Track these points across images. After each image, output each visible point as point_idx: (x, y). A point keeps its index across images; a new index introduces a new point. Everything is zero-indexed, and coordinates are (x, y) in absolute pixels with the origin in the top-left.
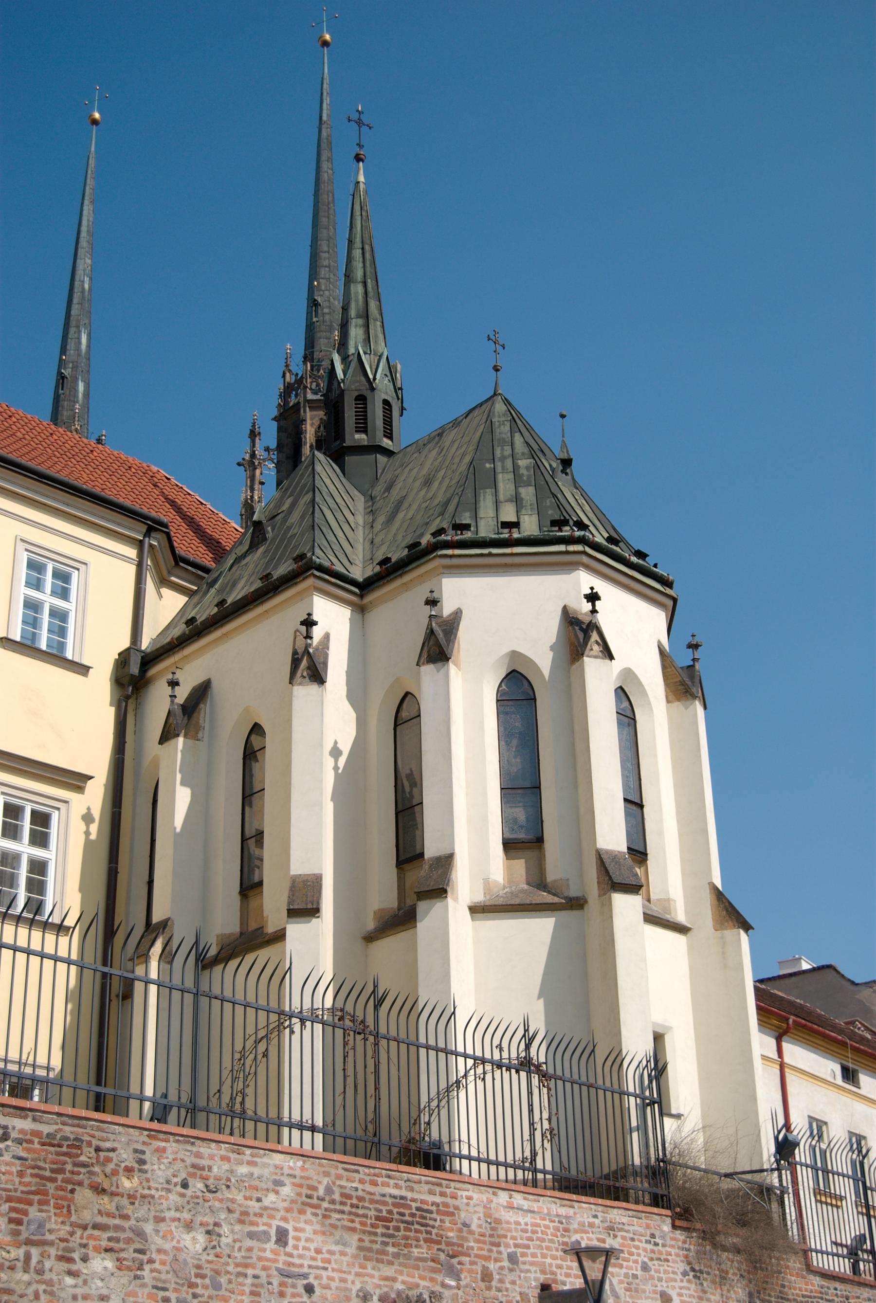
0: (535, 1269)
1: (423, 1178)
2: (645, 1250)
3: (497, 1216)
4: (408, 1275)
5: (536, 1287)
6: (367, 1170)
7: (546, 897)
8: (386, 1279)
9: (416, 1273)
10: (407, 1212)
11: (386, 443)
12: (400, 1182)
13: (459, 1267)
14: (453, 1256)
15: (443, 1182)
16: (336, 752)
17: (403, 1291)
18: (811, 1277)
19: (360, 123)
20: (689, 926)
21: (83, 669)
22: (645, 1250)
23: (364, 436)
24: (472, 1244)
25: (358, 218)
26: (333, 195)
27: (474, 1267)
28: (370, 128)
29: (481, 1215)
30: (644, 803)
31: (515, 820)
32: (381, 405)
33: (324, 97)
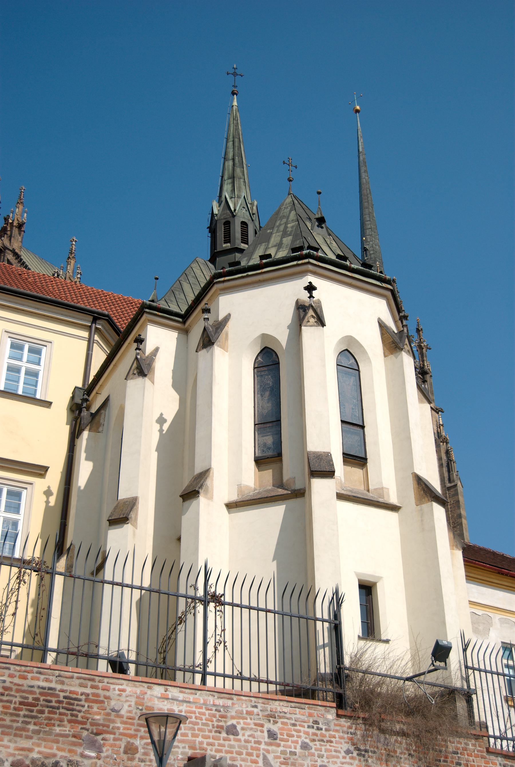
0: (183, 745)
1: (76, 675)
2: (307, 733)
3: (149, 704)
4: (45, 747)
5: (182, 759)
6: (18, 668)
7: (281, 491)
8: (23, 749)
9: (55, 746)
10: (54, 699)
11: (243, 246)
12: (51, 677)
13: (102, 742)
14: (97, 734)
15: (97, 678)
16: (161, 420)
17: (39, 760)
18: (492, 757)
19: (235, 74)
20: (399, 505)
21: (48, 404)
22: (307, 733)
23: (229, 244)
24: (119, 725)
25: (232, 125)
26: (370, 190)
27: (118, 743)
28: (242, 76)
29: (133, 704)
30: (365, 425)
31: (265, 445)
32: (240, 225)
33: (359, 139)
